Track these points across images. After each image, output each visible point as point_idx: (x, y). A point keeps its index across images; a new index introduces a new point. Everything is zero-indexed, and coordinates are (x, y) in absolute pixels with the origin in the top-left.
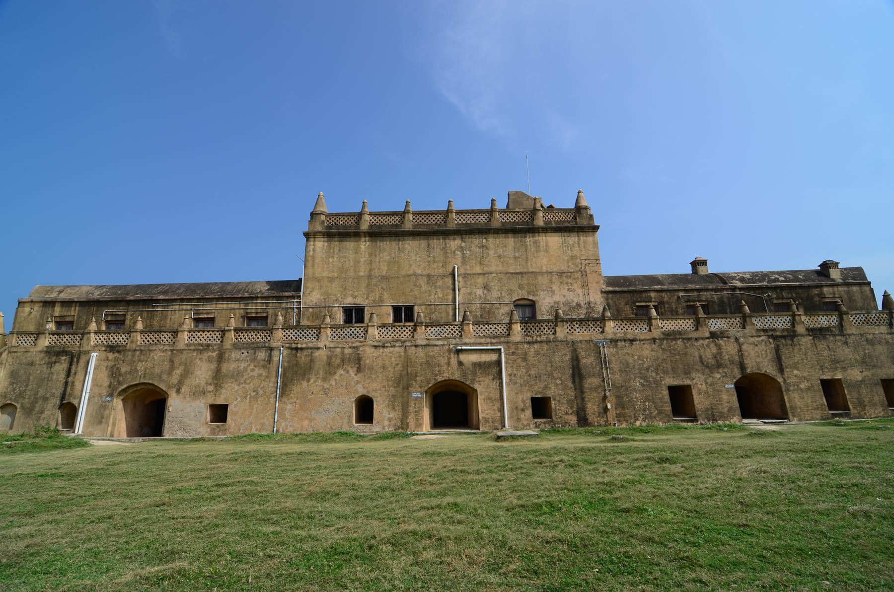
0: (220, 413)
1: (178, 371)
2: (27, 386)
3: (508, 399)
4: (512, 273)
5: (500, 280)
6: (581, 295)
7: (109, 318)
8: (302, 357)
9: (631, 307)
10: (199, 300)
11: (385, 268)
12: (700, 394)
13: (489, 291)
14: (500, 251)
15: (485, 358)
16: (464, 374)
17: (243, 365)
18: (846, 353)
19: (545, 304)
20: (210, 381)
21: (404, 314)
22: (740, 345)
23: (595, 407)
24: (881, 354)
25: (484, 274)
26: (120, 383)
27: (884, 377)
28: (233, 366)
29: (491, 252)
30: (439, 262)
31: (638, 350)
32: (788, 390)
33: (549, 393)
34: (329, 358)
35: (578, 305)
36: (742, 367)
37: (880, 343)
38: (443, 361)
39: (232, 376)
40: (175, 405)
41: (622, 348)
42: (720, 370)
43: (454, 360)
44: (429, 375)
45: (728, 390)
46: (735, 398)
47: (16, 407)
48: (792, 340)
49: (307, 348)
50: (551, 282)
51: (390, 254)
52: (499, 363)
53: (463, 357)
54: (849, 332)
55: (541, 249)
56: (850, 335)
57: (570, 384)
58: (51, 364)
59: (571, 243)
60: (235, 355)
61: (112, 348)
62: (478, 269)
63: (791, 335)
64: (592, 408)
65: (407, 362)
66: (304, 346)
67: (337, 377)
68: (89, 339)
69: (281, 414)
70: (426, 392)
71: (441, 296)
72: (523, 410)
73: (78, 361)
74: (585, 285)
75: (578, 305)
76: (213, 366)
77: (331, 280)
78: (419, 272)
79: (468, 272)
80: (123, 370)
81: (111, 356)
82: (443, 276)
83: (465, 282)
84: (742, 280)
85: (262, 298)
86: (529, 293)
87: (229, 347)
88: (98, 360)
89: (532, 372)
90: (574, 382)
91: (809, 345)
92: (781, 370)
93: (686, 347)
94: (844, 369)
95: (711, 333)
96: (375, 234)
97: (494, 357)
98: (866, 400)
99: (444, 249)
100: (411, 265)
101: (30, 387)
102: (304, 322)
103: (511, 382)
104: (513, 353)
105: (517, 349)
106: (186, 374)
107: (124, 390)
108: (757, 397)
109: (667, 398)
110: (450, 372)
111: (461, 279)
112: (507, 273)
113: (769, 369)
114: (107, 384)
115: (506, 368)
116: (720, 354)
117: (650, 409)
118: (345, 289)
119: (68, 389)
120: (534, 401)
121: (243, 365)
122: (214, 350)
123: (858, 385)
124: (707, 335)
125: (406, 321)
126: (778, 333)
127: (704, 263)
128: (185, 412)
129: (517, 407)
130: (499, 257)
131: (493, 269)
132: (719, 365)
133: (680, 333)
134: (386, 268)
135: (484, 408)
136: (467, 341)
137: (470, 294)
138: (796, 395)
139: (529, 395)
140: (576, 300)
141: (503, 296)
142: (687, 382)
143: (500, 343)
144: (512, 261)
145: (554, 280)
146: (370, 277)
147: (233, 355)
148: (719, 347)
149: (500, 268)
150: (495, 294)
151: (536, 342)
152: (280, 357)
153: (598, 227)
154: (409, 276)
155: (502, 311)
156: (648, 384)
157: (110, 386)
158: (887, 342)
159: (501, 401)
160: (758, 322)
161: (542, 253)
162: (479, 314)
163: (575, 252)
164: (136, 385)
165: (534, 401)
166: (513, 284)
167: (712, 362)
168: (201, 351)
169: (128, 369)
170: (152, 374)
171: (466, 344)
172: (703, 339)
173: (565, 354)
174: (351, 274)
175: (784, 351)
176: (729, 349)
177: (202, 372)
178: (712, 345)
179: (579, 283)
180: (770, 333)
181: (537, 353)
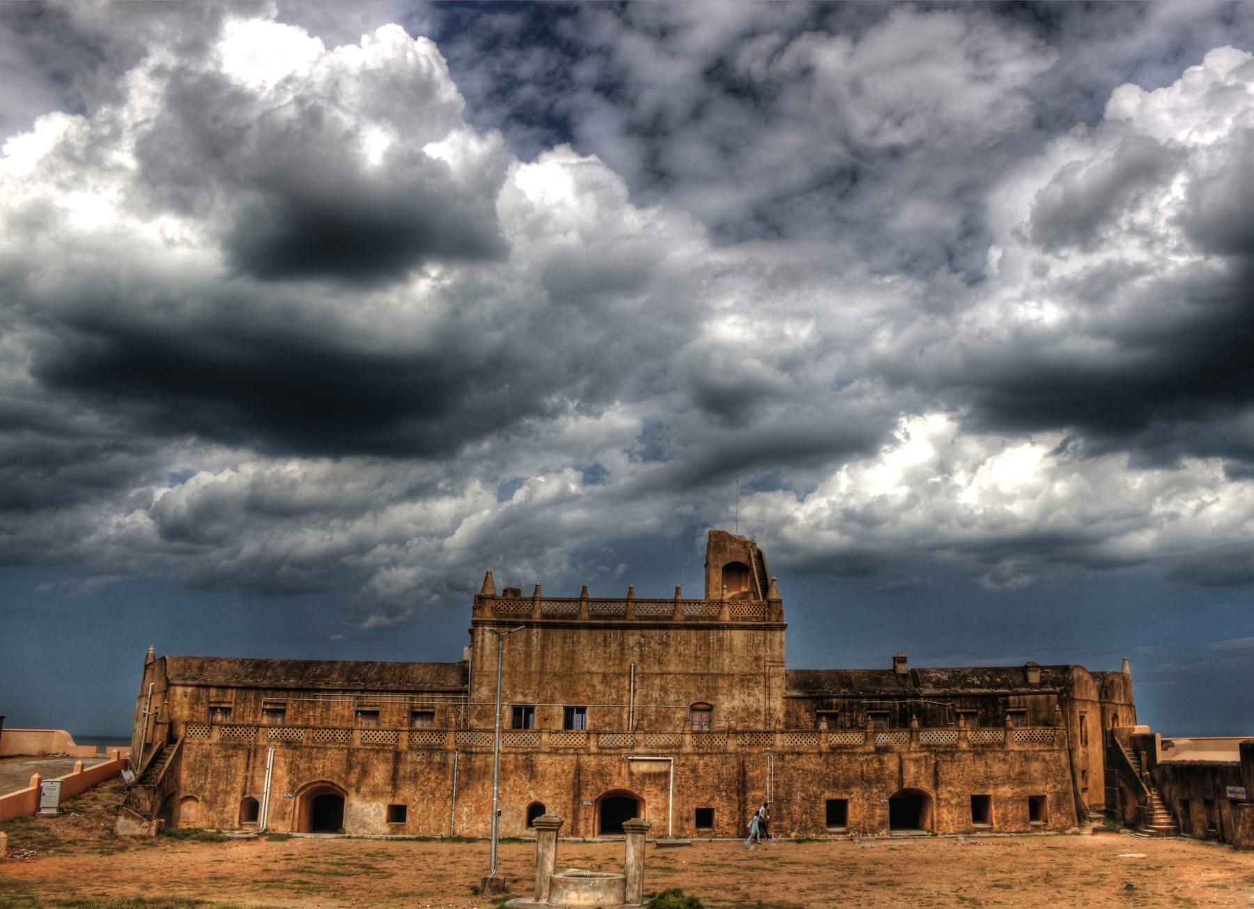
5: (679, 681)
6: (762, 699)
7: (268, 707)
8: (478, 762)
13: (666, 693)
14: (681, 648)
15: (655, 768)
17: (419, 767)
18: (998, 768)
26: (300, 780)
27: (1033, 794)
29: (672, 650)
33: (713, 805)
35: (758, 711)
36: (901, 781)
37: (1037, 760)
43: (624, 771)
46: (887, 812)
49: (482, 753)
52: (666, 774)
53: (634, 767)
57: (734, 796)
60: (411, 757)
62: (656, 669)
65: (579, 770)
67: (511, 783)
69: (458, 816)
72: (688, 820)
73: (255, 755)
75: (758, 711)
76: (390, 767)
80: (302, 766)
81: (289, 752)
82: (619, 675)
84: (938, 684)
86: (707, 697)
92: (936, 785)
94: (996, 786)
96: (550, 624)
99: (622, 645)
102: (340, 735)
103: (678, 793)
104: (683, 765)
106: (365, 773)
107: (303, 788)
108: (908, 811)
109: (824, 812)
110: (620, 783)
113: (925, 785)
114: (287, 780)
116: (881, 769)
118: (515, 686)
120: (699, 811)
121: (419, 767)
124: (872, 748)
128: (367, 813)
130: (680, 655)
131: (672, 668)
132: (879, 780)
137: (646, 696)
139: (695, 806)
142: (845, 796)
143: (671, 754)
144: (693, 661)
146: (541, 673)
148: (881, 762)
149: (680, 669)
150: (672, 697)
151: (707, 753)
152: (454, 759)
155: (678, 715)
158: (1044, 760)
159: (660, 810)
160: (925, 737)
161: (726, 654)
162: (653, 718)
165: (699, 811)
167: (873, 776)
168: (377, 752)
171: (637, 754)
172: (868, 754)
175: (944, 767)
177: (380, 773)
179: (761, 687)
181: (706, 765)
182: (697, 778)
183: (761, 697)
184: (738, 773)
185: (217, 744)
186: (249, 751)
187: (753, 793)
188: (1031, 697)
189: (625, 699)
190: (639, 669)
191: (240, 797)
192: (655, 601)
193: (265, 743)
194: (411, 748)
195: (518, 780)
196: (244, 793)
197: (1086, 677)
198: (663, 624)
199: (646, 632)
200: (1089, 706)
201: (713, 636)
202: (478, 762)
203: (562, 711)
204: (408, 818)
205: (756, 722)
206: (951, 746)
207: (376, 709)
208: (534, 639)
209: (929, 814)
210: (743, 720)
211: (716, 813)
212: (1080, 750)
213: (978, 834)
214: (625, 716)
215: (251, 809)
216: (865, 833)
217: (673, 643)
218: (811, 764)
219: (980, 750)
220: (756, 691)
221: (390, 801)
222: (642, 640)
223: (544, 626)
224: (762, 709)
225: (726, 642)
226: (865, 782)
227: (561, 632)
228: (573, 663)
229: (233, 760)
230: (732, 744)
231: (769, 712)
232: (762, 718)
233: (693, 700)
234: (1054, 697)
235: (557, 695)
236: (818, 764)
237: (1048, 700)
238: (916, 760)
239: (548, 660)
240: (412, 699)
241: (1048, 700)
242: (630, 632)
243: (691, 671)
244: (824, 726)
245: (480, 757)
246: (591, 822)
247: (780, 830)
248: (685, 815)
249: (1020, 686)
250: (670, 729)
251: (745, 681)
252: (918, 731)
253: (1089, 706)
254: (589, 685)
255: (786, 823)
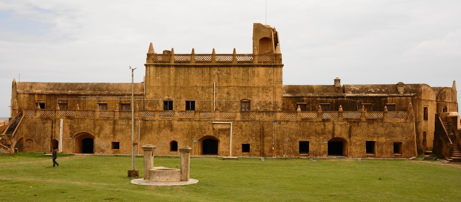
0: (116, 145)
1: (98, 128)
2: (35, 132)
3: (232, 144)
4: (241, 87)
5: (235, 90)
6: (272, 98)
7: (60, 102)
8: (148, 124)
9: (294, 105)
10: (99, 95)
11: (182, 83)
12: (312, 145)
14: (236, 76)
15: (224, 127)
16: (215, 133)
18: (381, 130)
19: (255, 100)
20: (111, 132)
21: (190, 106)
22: (334, 125)
23: (268, 149)
24: (398, 131)
25: (227, 87)
27: (396, 141)
28: (119, 127)
29: (232, 76)
30: (207, 80)
31: (290, 124)
32: (351, 145)
33: (249, 143)
34: (159, 125)
35: (270, 103)
36: (333, 134)
37: (398, 126)
38: (207, 128)
39: (120, 131)
40: (98, 142)
41: (283, 125)
42: (323, 136)
43: (211, 128)
44: (200, 134)
45: (324, 144)
46: (327, 147)
47: (33, 141)
48: (358, 124)
49: (150, 120)
50: (258, 91)
51: (184, 76)
52: (229, 129)
53: (215, 126)
54: (386, 121)
55: (255, 75)
56: (385, 122)
57: (259, 139)
58: (44, 123)
59: (270, 72)
60: (120, 122)
61: (68, 117)
62: (225, 84)
63: (357, 122)
64: (266, 149)
66: (148, 119)
67: (163, 132)
68: (58, 113)
70: (199, 140)
71: (207, 97)
72: (238, 149)
74: (274, 94)
75: (270, 103)
76: (112, 127)
77: (158, 88)
78: (198, 85)
79: (221, 86)
80: (75, 127)
81: (69, 121)
82: (209, 87)
83: (219, 90)
84: (354, 92)
85: (127, 95)
86: (248, 97)
87: (117, 118)
88: (63, 122)
89: (244, 134)
90: (260, 138)
91: (365, 126)
92: (350, 137)
93: (310, 125)
94: (378, 137)
95: (323, 119)
97: (227, 127)
98: (384, 150)
100: (194, 82)
101: (37, 133)
103: (234, 137)
104: (236, 125)
105: (238, 123)
106: (101, 129)
107: (76, 135)
108: (337, 148)
109: (298, 146)
110: (210, 133)
111: (217, 89)
112: (238, 87)
113: (345, 136)
115: (233, 132)
116: (325, 129)
117: (290, 150)
118: (164, 92)
119: (53, 134)
121: (123, 127)
122: (111, 120)
123: (382, 144)
124: (321, 120)
125: (192, 110)
126: (353, 121)
127: (339, 80)
129: (236, 148)
130: (235, 78)
131: (232, 84)
132: (323, 133)
133: (309, 119)
134: (183, 83)
135: (221, 147)
136: (217, 119)
137: (221, 96)
138: (354, 147)
139: (241, 143)
140: (269, 101)
141: (236, 98)
142: (308, 140)
143: (230, 121)
144: (241, 81)
145: (260, 90)
146: (175, 86)
147: (119, 122)
148: (325, 125)
149: (235, 84)
150: (232, 97)
151: (247, 121)
153: (283, 65)
154: (193, 87)
155: (235, 105)
156: (291, 140)
157: (70, 133)
158: (402, 127)
159: (228, 145)
161: (256, 78)
162: (224, 105)
163: (271, 77)
164: (81, 133)
166: (241, 92)
167: (321, 132)
168: (106, 120)
169: (77, 126)
170: (87, 129)
171: (216, 121)
173: (258, 127)
174: (167, 85)
175: (354, 128)
176: (329, 126)
177: (108, 129)
178: (322, 125)
179: (272, 92)
180: (349, 120)
181: (246, 126)
182: (242, 132)
183: (272, 97)
184: (260, 129)
185: (39, 118)
186: (53, 121)
187: (267, 138)
188: (399, 98)
189: (212, 97)
190: (218, 85)
191: (50, 139)
192: (224, 55)
193: (59, 117)
194: (120, 118)
195: (166, 132)
196: (52, 138)
197: (429, 89)
198: (211, 66)
199: (221, 68)
200: (430, 103)
201: (250, 69)
202: (148, 124)
203: (185, 103)
204: (120, 148)
205: (270, 108)
206: (357, 119)
207: (106, 102)
208: (172, 72)
209: (346, 148)
210: (263, 106)
211: (251, 146)
212: (423, 123)
213: (369, 158)
214: (212, 105)
215: (55, 144)
216: (316, 156)
217: (232, 73)
218: (293, 126)
219: (371, 121)
220: (269, 94)
221: (112, 140)
222: (219, 72)
223: (176, 66)
224: (272, 102)
225: (256, 73)
226: (317, 134)
227: (183, 69)
228: (189, 82)
229: (46, 125)
230: (257, 117)
231: (275, 104)
232: (272, 106)
233: (241, 98)
234: (410, 98)
235: (182, 96)
236: (296, 126)
237: (407, 100)
238: (341, 125)
239: (177, 81)
240: (121, 98)
241: (407, 100)
242: (213, 68)
243: (241, 85)
244: (299, 109)
245: (149, 122)
246: (197, 149)
247: (278, 153)
248: (238, 147)
249: (394, 93)
250: (231, 110)
251: (265, 89)
252: (342, 112)
253: (430, 103)
254: (196, 91)
255: (281, 151)
